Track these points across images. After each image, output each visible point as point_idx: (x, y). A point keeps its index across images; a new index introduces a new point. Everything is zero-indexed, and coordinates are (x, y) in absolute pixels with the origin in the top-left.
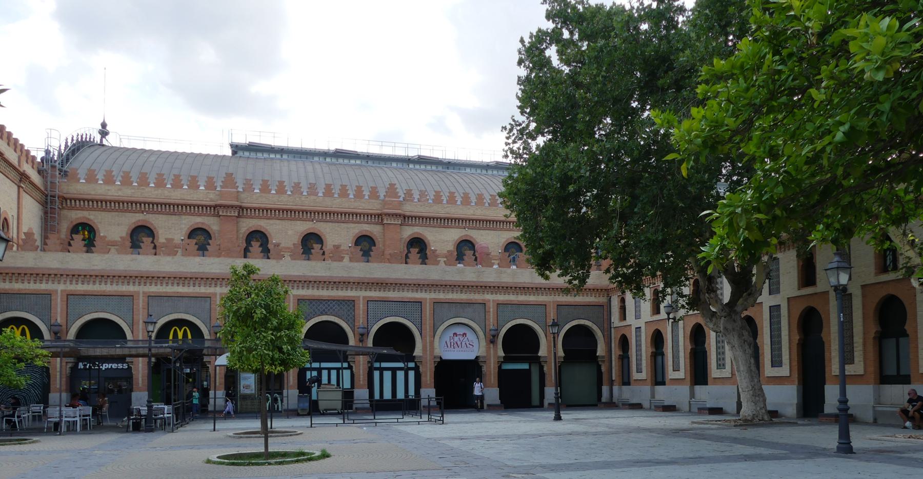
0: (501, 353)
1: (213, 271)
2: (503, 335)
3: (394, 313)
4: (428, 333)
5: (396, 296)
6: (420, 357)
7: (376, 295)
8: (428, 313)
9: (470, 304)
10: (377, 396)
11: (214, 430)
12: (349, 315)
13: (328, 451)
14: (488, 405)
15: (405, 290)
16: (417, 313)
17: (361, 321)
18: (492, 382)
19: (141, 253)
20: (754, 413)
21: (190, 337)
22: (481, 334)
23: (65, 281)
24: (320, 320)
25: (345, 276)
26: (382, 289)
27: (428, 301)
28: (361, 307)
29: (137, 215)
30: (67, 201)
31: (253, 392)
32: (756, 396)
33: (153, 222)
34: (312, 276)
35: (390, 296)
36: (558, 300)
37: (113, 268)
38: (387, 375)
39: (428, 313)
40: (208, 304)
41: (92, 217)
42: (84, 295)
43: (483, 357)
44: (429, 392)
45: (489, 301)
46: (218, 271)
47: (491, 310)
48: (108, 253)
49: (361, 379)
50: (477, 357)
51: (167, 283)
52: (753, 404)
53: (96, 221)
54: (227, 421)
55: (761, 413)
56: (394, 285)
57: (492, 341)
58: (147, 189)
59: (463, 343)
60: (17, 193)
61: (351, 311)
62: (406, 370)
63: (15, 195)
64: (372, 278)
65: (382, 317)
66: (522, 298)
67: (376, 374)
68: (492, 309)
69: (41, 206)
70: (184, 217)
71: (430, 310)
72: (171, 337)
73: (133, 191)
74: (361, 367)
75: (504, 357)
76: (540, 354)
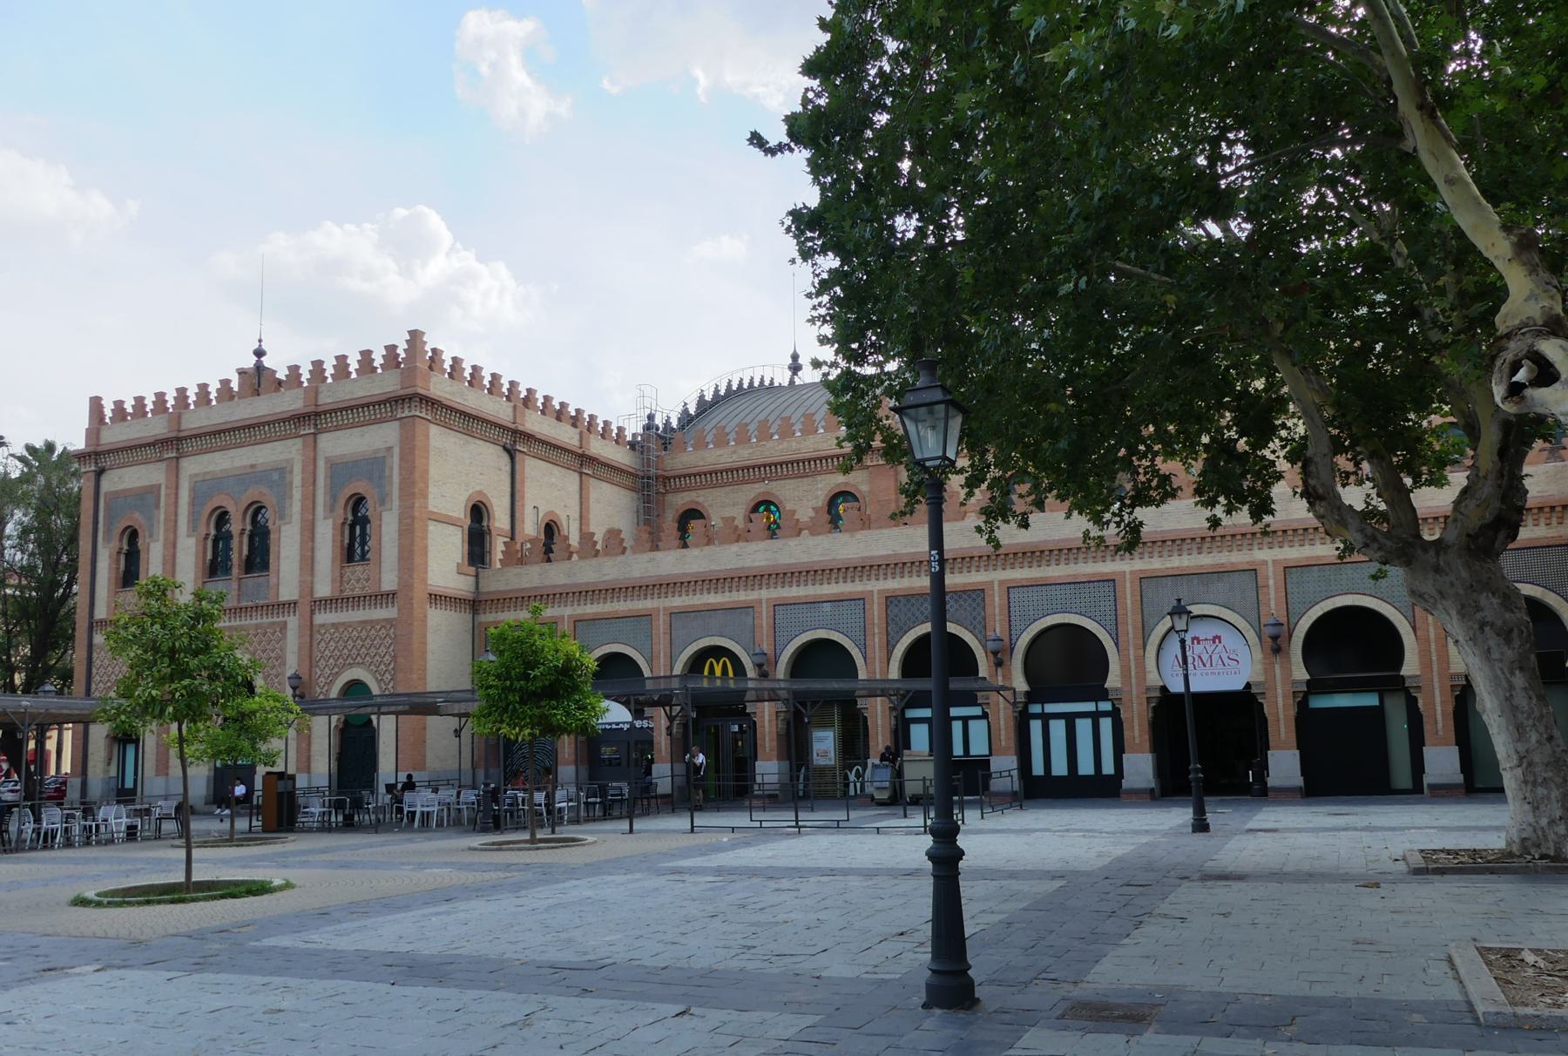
0: (1301, 674)
1: (757, 564)
2: (1302, 635)
3: (1054, 606)
4: (1131, 642)
5: (1062, 574)
6: (1117, 689)
7: (1024, 576)
8: (1129, 602)
9: (1220, 573)
10: (1038, 769)
11: (631, 831)
12: (975, 618)
13: (292, 881)
14: (1433, 787)
15: (1080, 560)
16: (1107, 603)
17: (998, 628)
18: (1283, 736)
19: (660, 547)
20: (1528, 833)
21: (731, 674)
22: (1251, 635)
23: (1150, 553)
24: (1066, 621)
25: (965, 546)
26: (1035, 564)
27: (1128, 576)
28: (996, 600)
29: (757, 486)
30: (667, 482)
31: (833, 763)
32: (1535, 784)
33: (778, 493)
34: (907, 554)
35: (1051, 574)
36: (886, 587)
37: (627, 576)
38: (1058, 729)
39: (1129, 602)
40: (750, 618)
41: (701, 499)
42: (595, 620)
43: (1259, 684)
44: (1140, 768)
45: (1265, 563)
46: (763, 563)
47: (1271, 582)
48: (963, 519)
49: (1002, 737)
50: (1248, 685)
51: (978, 567)
52: (1527, 807)
53: (706, 504)
54: (720, 814)
55: (1552, 837)
56: (1179, 542)
57: (1276, 645)
58: (770, 444)
59: (1216, 658)
60: (578, 483)
61: (979, 609)
62: (1095, 717)
63: (576, 487)
64: (1013, 545)
65: (1036, 617)
66: (713, 599)
67: (1036, 727)
68: (1272, 581)
69: (635, 495)
70: (819, 478)
71: (1133, 596)
72: (706, 673)
73: (751, 451)
74: (1002, 714)
75: (1308, 682)
76: (1107, 685)
